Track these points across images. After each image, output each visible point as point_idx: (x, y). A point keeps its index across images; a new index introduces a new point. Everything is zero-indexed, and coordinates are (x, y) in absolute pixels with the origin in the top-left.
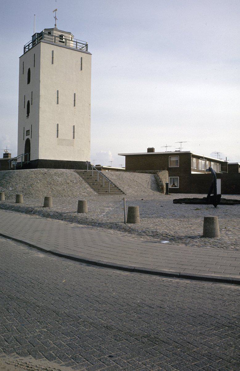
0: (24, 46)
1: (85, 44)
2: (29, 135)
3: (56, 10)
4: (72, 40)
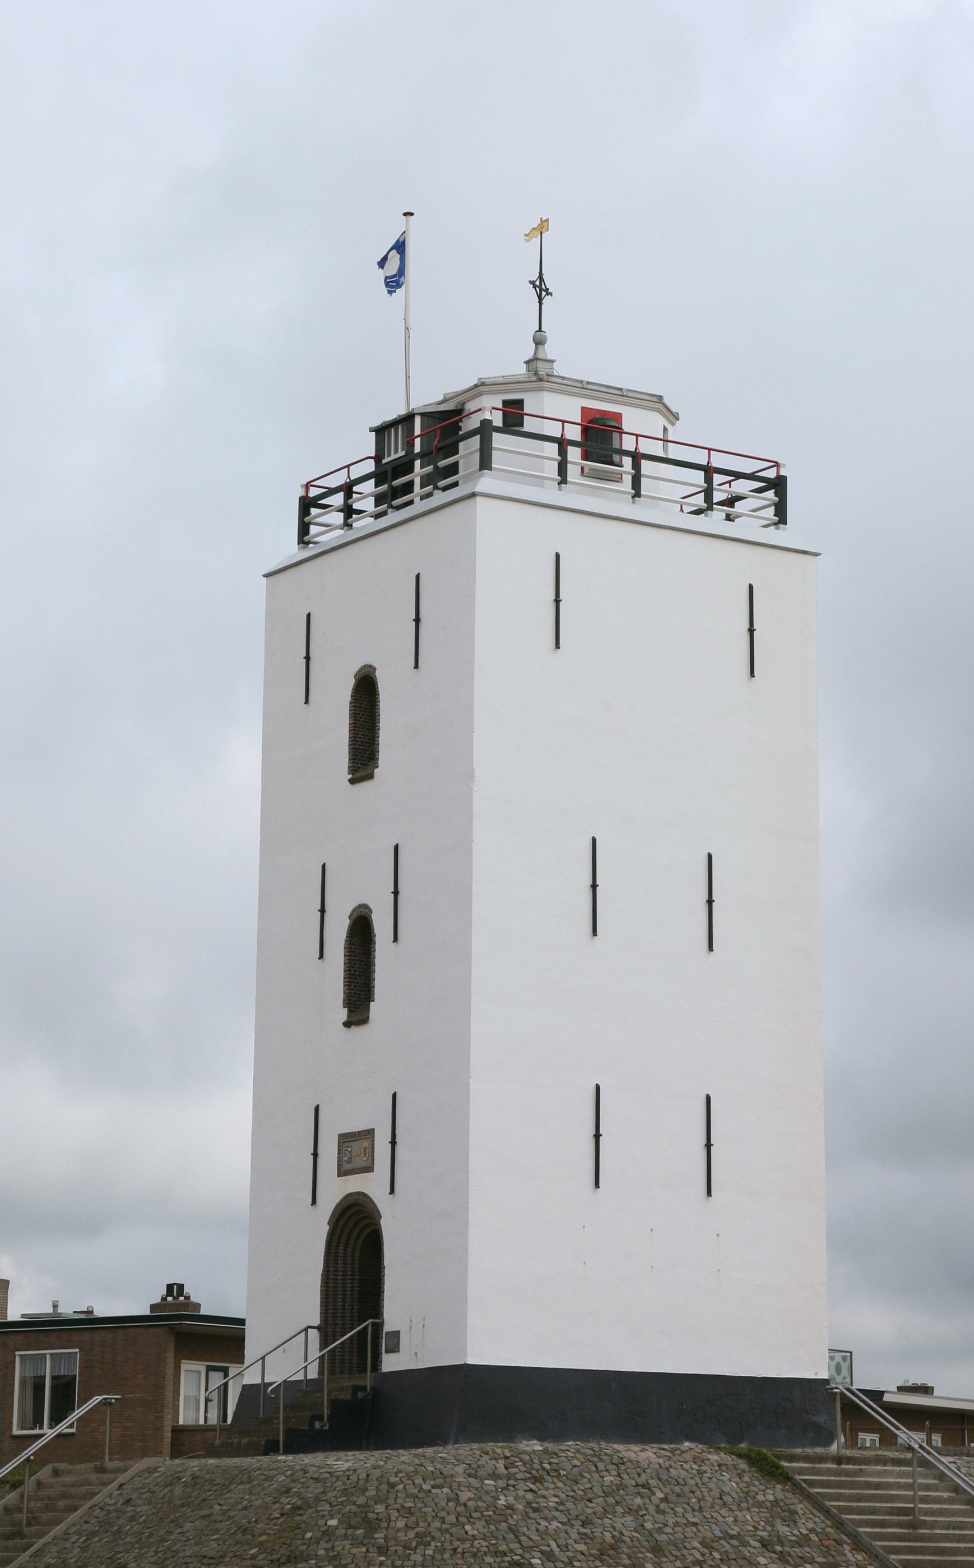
0: (301, 492)
1: (752, 477)
2: (369, 1169)
3: (543, 227)
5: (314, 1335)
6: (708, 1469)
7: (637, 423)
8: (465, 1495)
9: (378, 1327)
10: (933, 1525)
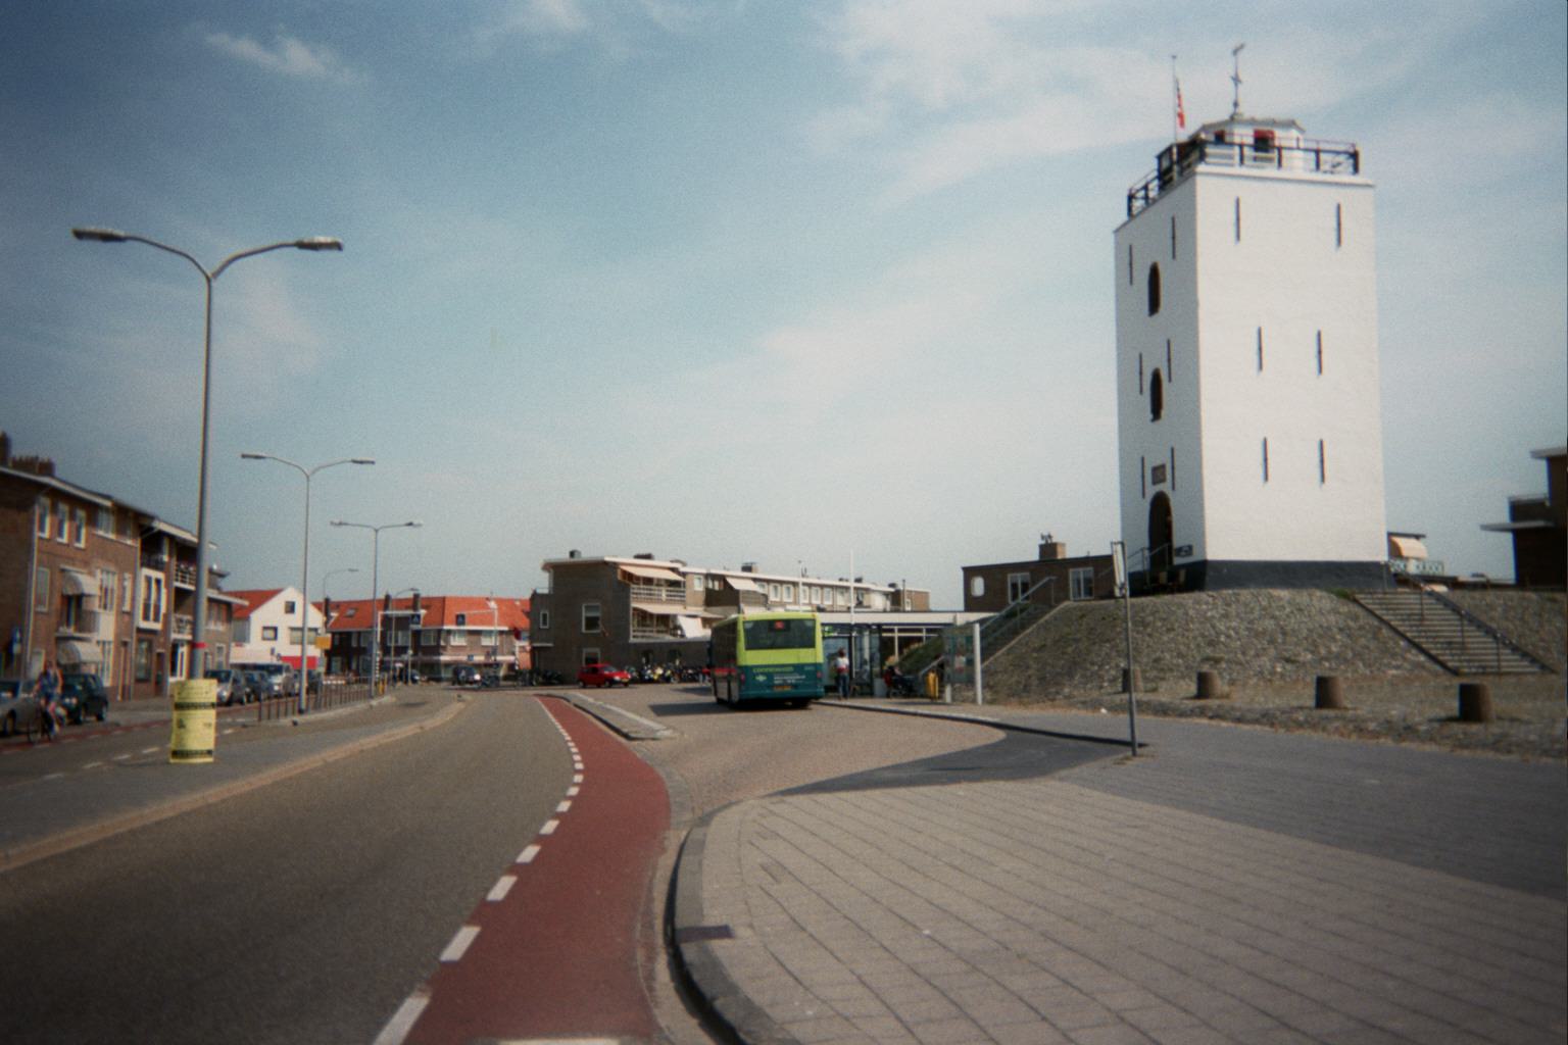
4: (1298, 148)
5: (1147, 553)
6: (1319, 601)
7: (1281, 137)
8: (1191, 612)
9: (1170, 547)
10: (1432, 620)
